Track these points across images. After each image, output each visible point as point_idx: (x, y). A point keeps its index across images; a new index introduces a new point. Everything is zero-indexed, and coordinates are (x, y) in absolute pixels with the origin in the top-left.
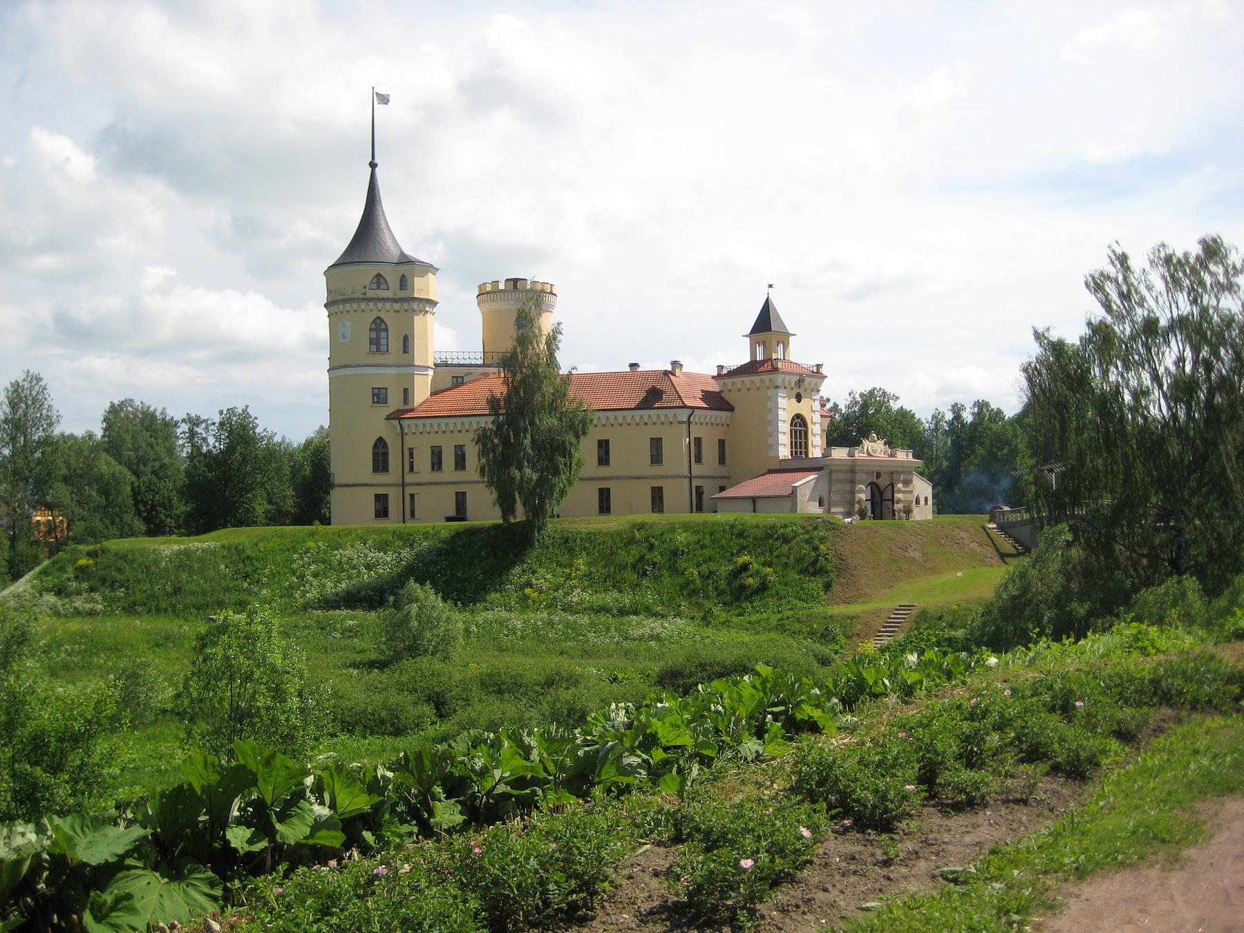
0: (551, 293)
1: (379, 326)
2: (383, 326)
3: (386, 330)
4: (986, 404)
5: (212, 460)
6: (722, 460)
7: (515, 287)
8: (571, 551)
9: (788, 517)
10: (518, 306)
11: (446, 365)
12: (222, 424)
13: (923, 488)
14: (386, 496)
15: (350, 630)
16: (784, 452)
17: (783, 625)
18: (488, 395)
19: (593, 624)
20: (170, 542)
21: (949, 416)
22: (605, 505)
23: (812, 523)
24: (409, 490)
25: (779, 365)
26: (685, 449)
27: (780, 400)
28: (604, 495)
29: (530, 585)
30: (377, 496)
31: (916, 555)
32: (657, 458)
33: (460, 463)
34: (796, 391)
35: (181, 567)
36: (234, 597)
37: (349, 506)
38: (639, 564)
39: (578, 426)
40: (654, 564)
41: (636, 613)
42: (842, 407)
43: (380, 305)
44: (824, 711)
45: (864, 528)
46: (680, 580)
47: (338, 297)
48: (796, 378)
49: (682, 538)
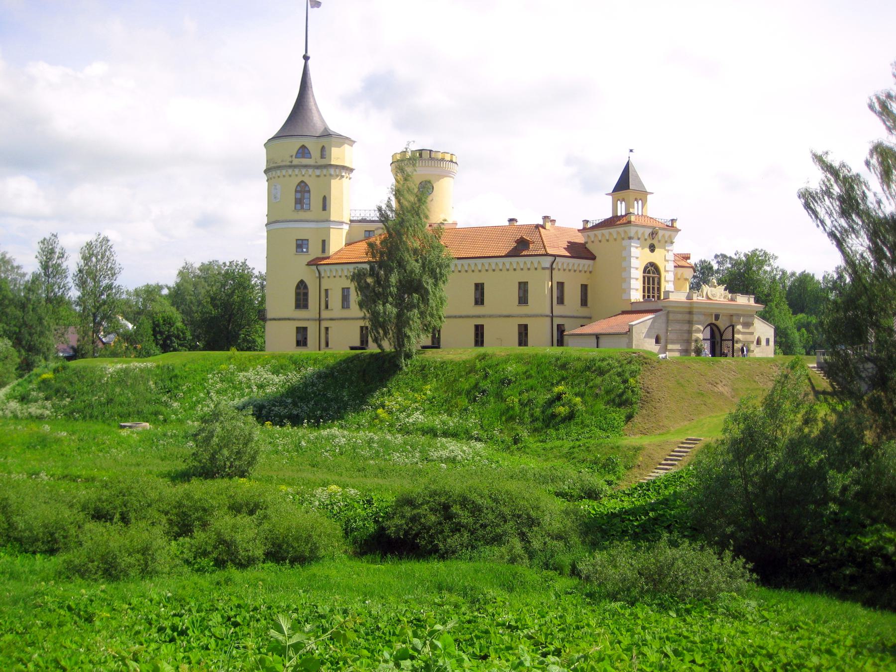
0: (451, 161)
1: (303, 190)
2: (307, 189)
3: (309, 191)
6: (584, 302)
13: (764, 330)
14: (305, 329)
16: (637, 295)
24: (324, 324)
26: (547, 292)
27: (633, 249)
32: (523, 300)
34: (649, 242)
36: (152, 408)
37: (278, 337)
43: (304, 171)
46: (503, 406)
48: (650, 231)
49: (511, 368)
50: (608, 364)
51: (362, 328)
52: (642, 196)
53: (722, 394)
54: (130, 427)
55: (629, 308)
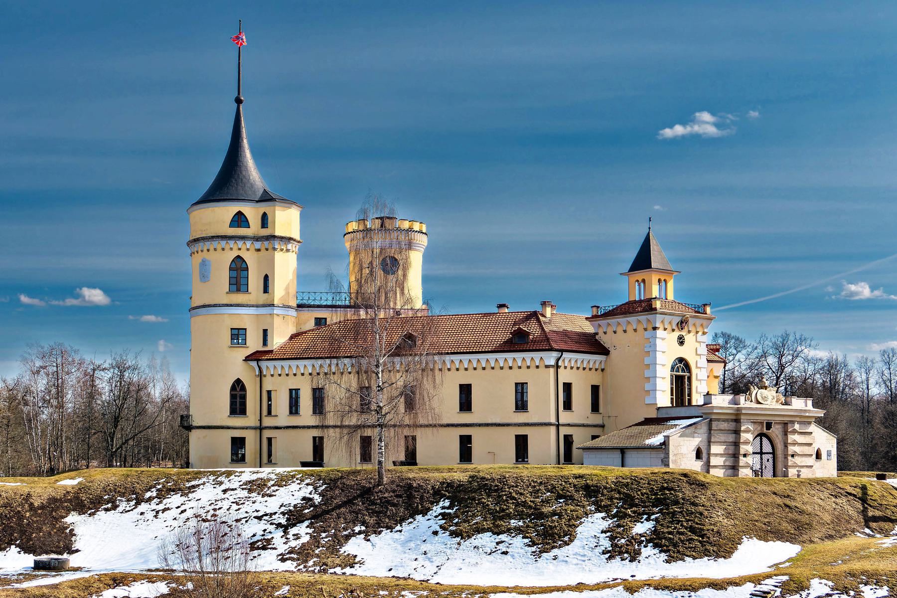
2: (244, 266)
3: (247, 269)
6: (595, 408)
16: (664, 398)
30: (518, 437)
32: (521, 405)
43: (240, 243)
48: (678, 319)
51: (314, 438)
55: (653, 415)
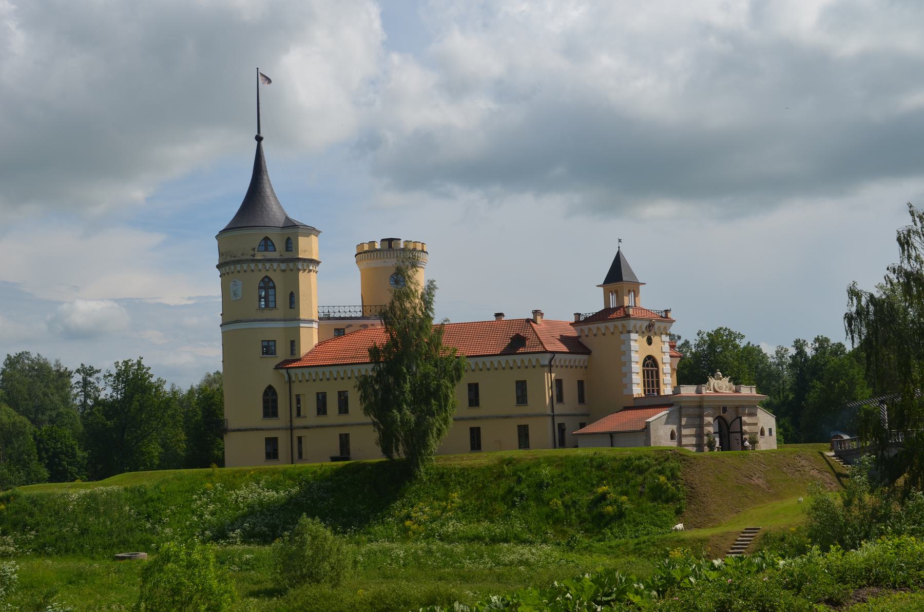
0: (423, 251)
1: (267, 284)
2: (271, 284)
3: (274, 287)
4: (827, 340)
5: (108, 408)
6: (581, 399)
7: (390, 246)
8: (446, 485)
9: (642, 450)
10: (392, 262)
11: (329, 318)
12: (118, 375)
13: (766, 420)
14: (275, 440)
15: (247, 563)
16: (638, 390)
17: (640, 549)
18: (371, 344)
19: (467, 552)
20: (76, 487)
21: (793, 351)
22: (476, 443)
23: (664, 456)
24: (297, 433)
25: (631, 311)
28: (475, 434)
29: (409, 517)
30: (519, 427)
31: (760, 482)
32: (522, 398)
33: (343, 408)
35: (87, 509)
37: (241, 450)
38: (508, 496)
39: (453, 370)
40: (522, 496)
41: (506, 540)
42: (692, 343)
43: (268, 265)
44: (642, 598)
45: (712, 458)
46: (545, 510)
47: (229, 259)
48: (647, 323)
49: (546, 471)
50: (646, 462)
52: (635, 287)
53: (758, 486)
54: (130, 558)
